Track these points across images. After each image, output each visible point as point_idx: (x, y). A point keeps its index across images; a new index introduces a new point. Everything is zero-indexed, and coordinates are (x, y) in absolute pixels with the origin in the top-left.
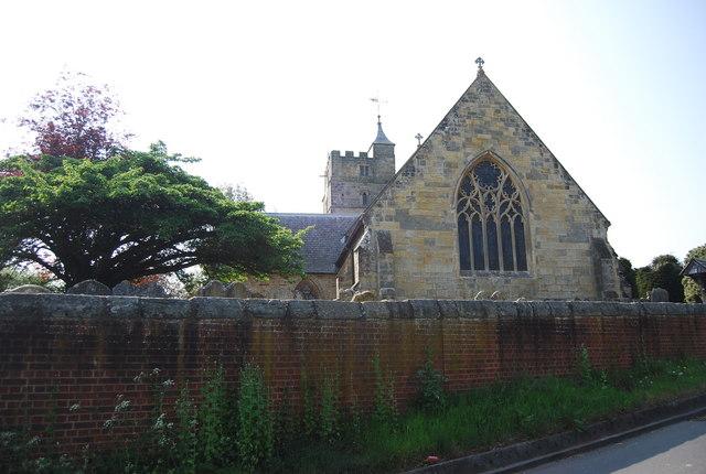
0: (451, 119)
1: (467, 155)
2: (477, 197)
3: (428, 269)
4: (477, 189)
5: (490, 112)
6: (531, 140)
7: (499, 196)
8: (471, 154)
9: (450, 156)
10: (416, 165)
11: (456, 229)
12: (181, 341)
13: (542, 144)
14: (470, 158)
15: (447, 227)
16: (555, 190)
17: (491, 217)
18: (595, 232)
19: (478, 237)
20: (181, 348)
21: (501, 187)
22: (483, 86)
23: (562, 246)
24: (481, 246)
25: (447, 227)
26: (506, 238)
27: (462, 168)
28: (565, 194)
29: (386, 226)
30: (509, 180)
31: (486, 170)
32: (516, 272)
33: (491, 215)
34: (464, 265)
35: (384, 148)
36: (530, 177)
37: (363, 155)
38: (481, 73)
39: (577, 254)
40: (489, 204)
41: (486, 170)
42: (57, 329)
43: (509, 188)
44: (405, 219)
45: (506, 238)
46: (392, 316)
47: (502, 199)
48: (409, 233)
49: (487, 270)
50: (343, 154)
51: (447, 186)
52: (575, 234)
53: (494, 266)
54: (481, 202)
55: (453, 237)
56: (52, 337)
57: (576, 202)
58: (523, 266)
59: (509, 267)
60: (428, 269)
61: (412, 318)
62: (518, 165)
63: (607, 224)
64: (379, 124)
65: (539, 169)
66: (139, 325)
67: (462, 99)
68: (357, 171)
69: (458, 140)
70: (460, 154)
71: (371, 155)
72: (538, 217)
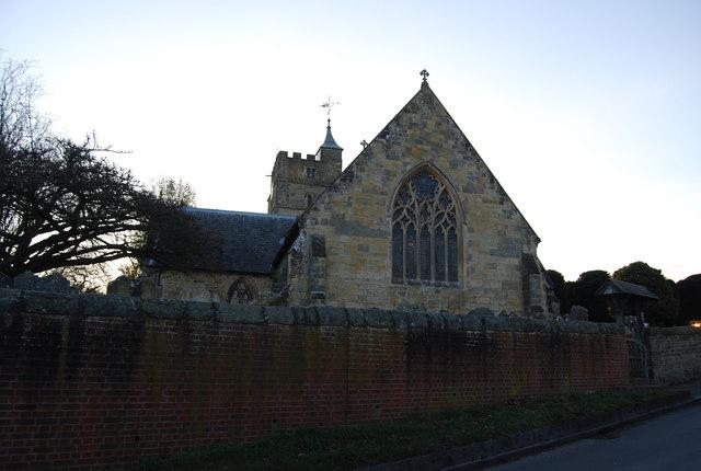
1: (405, 164)
2: (413, 206)
4: (413, 199)
5: (431, 125)
6: (469, 154)
8: (411, 164)
9: (389, 164)
14: (409, 168)
21: (437, 197)
25: (382, 234)
27: (400, 177)
29: (322, 230)
30: (445, 191)
31: (424, 177)
33: (425, 225)
34: (396, 272)
35: (331, 150)
37: (310, 157)
38: (425, 85)
40: (425, 213)
41: (424, 177)
43: (445, 199)
45: (439, 249)
46: (296, 323)
48: (344, 238)
52: (506, 248)
54: (417, 212)
57: (509, 217)
58: (454, 276)
60: (361, 275)
67: (405, 110)
70: (400, 163)
71: (318, 158)
72: (471, 230)
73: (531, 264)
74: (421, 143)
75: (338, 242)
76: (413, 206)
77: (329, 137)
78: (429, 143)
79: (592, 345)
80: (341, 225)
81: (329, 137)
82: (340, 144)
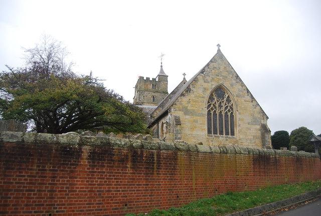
0: (206, 69)
1: (212, 85)
3: (195, 133)
4: (215, 100)
5: (222, 68)
6: (238, 80)
7: (224, 103)
8: (214, 85)
9: (206, 85)
10: (191, 87)
11: (206, 117)
12: (155, 159)
13: (242, 83)
14: (214, 86)
15: (203, 115)
16: (248, 103)
17: (221, 112)
18: (262, 121)
19: (215, 120)
20: (155, 161)
21: (225, 99)
22: (219, 57)
23: (249, 126)
24: (216, 124)
25: (203, 115)
26: (227, 121)
28: (251, 104)
30: (228, 97)
31: (219, 91)
32: (230, 136)
34: (209, 132)
35: (163, 78)
36: (237, 96)
37: (154, 80)
38: (219, 51)
39: (255, 130)
40: (220, 106)
41: (219, 91)
42: (115, 152)
43: (228, 100)
44: (186, 112)
45: (227, 121)
46: (221, 152)
47: (226, 104)
48: (187, 117)
49: (218, 135)
50: (145, 79)
51: (203, 97)
52: (255, 122)
53: (221, 133)
55: (205, 120)
56: (114, 155)
57: (255, 108)
58: (233, 134)
59: (227, 134)
60: (195, 133)
61: (227, 153)
62: (233, 90)
63: (267, 118)
64: (161, 66)
65: (241, 93)
66: (142, 152)
67: (211, 61)
68: (151, 87)
69: (209, 79)
70: (210, 84)
71: (157, 80)
72: (240, 114)
73: (265, 129)
74: (218, 76)
75: (185, 119)
76: (215, 102)
77: (162, 71)
78: (222, 76)
79: (309, 162)
80: (186, 112)
81: (162, 71)
82: (166, 73)
